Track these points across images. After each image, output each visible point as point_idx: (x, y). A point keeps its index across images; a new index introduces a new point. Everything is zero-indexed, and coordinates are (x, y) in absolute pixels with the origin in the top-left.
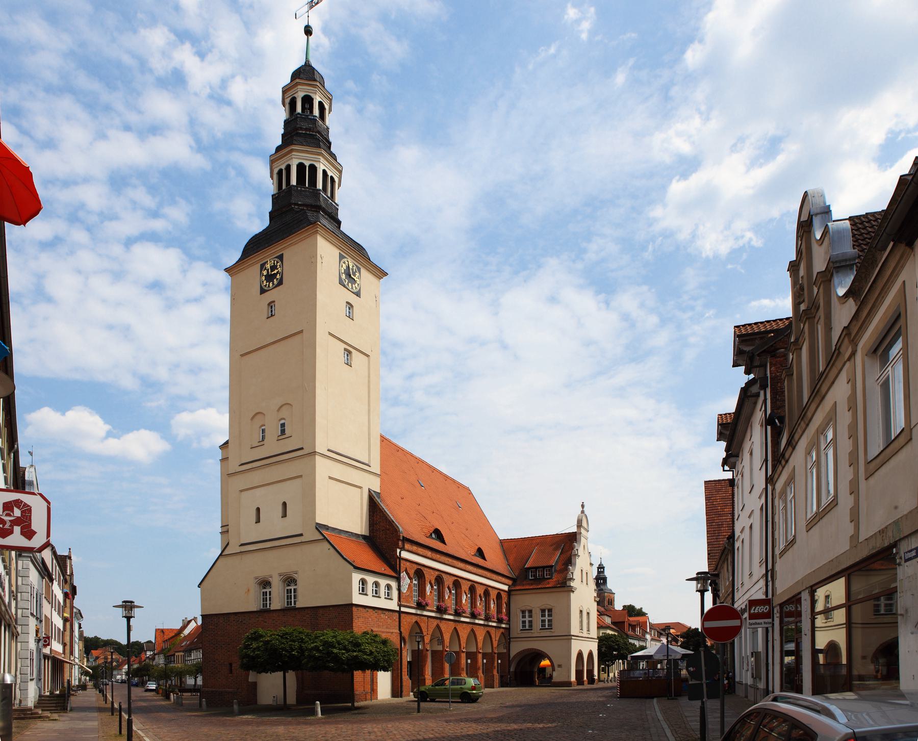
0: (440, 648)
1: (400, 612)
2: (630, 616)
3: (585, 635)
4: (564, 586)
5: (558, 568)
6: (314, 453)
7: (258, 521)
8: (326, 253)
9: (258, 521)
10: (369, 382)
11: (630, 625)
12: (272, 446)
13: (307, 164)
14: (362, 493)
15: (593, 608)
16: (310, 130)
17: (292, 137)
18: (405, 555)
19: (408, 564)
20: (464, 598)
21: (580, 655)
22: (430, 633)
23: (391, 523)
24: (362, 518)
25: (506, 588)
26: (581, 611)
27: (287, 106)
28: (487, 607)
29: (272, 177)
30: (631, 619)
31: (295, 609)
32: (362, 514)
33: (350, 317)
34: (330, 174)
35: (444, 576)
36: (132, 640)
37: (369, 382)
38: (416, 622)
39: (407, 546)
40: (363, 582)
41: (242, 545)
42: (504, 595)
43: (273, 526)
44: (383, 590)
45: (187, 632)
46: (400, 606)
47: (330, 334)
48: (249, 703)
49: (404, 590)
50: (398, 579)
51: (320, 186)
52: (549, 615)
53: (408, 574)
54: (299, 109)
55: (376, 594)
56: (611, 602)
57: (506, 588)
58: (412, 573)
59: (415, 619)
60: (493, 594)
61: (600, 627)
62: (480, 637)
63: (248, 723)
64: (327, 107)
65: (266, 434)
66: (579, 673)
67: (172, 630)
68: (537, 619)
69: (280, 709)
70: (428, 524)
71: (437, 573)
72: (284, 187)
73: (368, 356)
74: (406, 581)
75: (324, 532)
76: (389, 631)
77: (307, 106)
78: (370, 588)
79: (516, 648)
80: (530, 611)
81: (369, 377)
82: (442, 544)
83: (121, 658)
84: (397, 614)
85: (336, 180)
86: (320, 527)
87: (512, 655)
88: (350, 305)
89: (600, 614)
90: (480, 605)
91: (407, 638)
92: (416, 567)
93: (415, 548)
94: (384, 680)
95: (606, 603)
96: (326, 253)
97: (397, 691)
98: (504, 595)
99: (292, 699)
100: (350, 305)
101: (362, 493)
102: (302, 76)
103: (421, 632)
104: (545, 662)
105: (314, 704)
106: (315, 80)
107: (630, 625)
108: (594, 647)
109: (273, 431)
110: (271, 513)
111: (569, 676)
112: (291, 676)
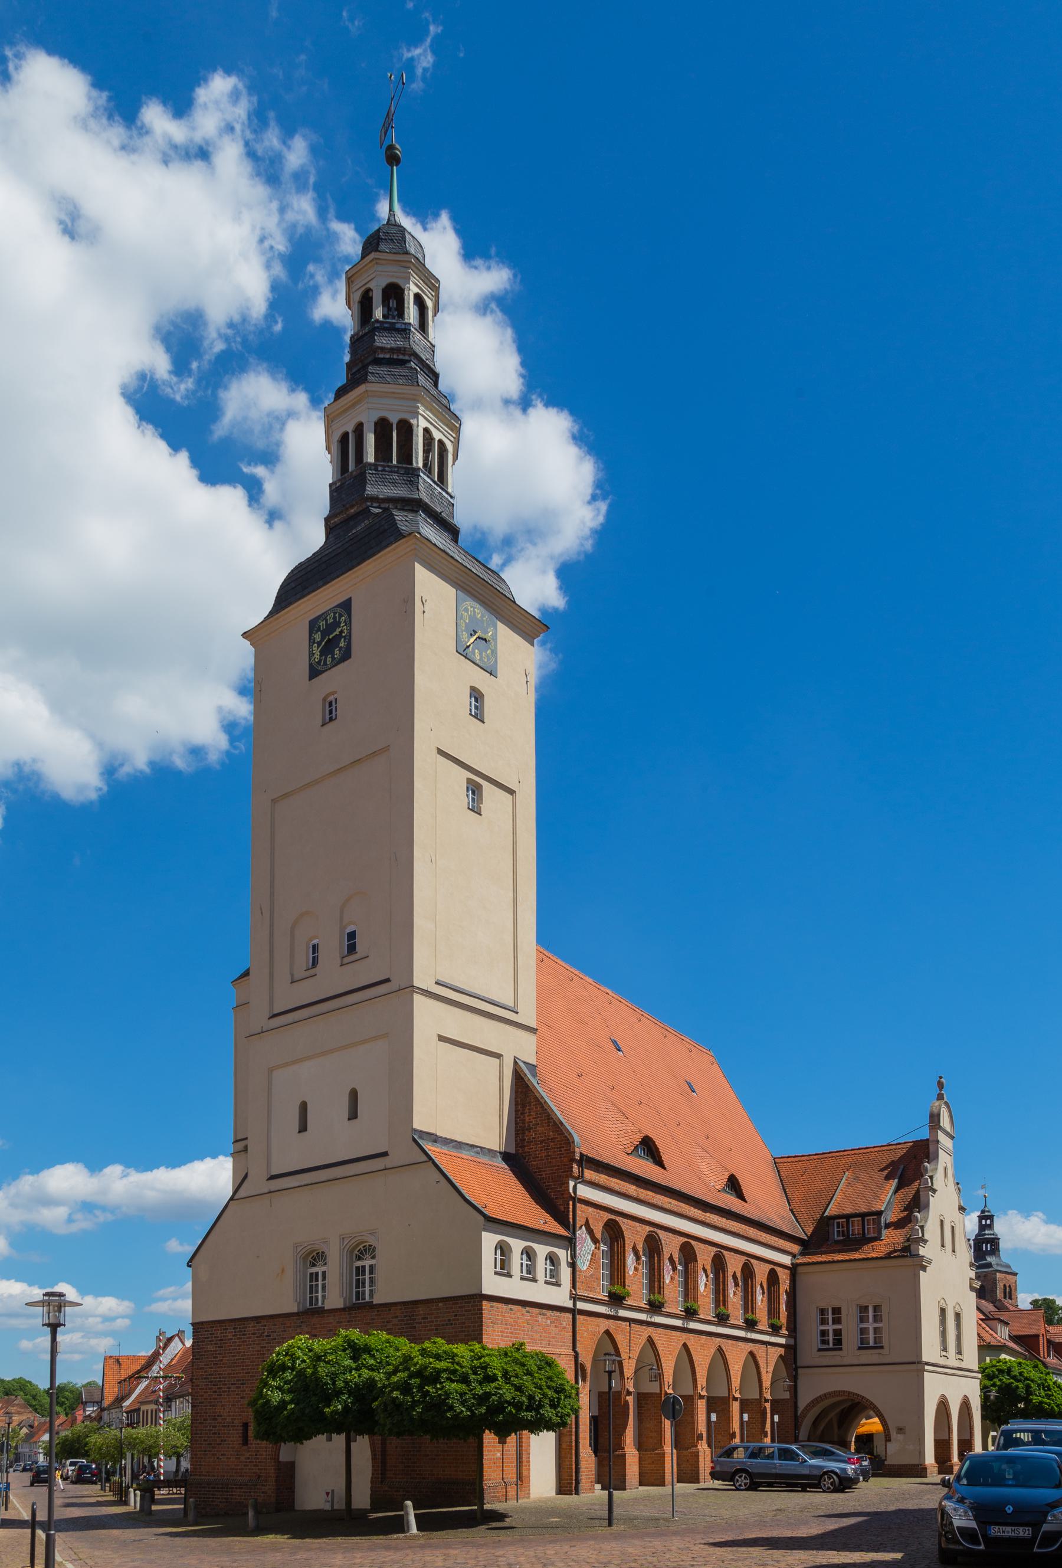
0: (654, 1388)
1: (574, 1312)
2: (1049, 1322)
3: (952, 1362)
4: (909, 1255)
5: (890, 1217)
6: (411, 988)
7: (303, 1128)
8: (435, 598)
9: (303, 1128)
10: (515, 843)
11: (1049, 1342)
12: (333, 976)
13: (394, 419)
14: (501, 1066)
15: (969, 1304)
16: (398, 350)
17: (365, 367)
18: (584, 1192)
19: (591, 1210)
20: (702, 1280)
21: (943, 1406)
22: (635, 1355)
23: (557, 1127)
24: (501, 1116)
25: (786, 1260)
26: (943, 1311)
27: (356, 306)
28: (748, 1303)
29: (328, 448)
30: (1052, 1329)
31: (371, 1306)
32: (501, 1110)
33: (478, 715)
34: (437, 435)
35: (662, 1234)
36: (58, 1382)
37: (515, 843)
38: (607, 1332)
39: (589, 1174)
40: (503, 1249)
41: (273, 1177)
42: (784, 1276)
43: (334, 1137)
44: (542, 1266)
45: (165, 1359)
46: (574, 1298)
47: (441, 752)
48: (280, 1512)
49: (583, 1265)
50: (570, 1243)
51: (419, 462)
52: (876, 1319)
53: (590, 1232)
54: (378, 313)
55: (529, 1275)
56: (1009, 1293)
57: (786, 1260)
58: (598, 1230)
59: (604, 1325)
60: (761, 1272)
61: (985, 1348)
62: (736, 1369)
63: (275, 1548)
64: (429, 304)
65: (321, 954)
66: (942, 1447)
67: (136, 1358)
68: (850, 1327)
69: (342, 1522)
70: (630, 1127)
71: (648, 1228)
72: (351, 466)
73: (511, 792)
74: (586, 1247)
75: (428, 1147)
76: (550, 1342)
77: (393, 303)
78: (517, 1260)
79: (814, 1387)
80: (837, 1311)
81: (514, 833)
82: (657, 1169)
83: (38, 1420)
84: (570, 1316)
85: (450, 446)
86: (418, 1138)
87: (802, 1405)
88: (476, 695)
89: (987, 1319)
90: (734, 1296)
91: (588, 1366)
92: (607, 1216)
93: (602, 1178)
94: (542, 1447)
95: (999, 1295)
96: (435, 598)
97: (567, 1483)
98: (784, 1276)
99: (362, 1499)
100: (476, 695)
101: (501, 1066)
102: (382, 246)
103: (618, 1353)
104: (871, 1425)
105: (401, 1507)
106: (407, 253)
107: (1049, 1342)
108: (971, 1389)
109: (332, 949)
110: (327, 1113)
111: (921, 1453)
112: (362, 1446)
